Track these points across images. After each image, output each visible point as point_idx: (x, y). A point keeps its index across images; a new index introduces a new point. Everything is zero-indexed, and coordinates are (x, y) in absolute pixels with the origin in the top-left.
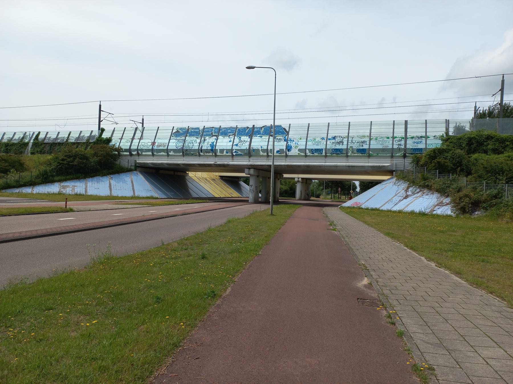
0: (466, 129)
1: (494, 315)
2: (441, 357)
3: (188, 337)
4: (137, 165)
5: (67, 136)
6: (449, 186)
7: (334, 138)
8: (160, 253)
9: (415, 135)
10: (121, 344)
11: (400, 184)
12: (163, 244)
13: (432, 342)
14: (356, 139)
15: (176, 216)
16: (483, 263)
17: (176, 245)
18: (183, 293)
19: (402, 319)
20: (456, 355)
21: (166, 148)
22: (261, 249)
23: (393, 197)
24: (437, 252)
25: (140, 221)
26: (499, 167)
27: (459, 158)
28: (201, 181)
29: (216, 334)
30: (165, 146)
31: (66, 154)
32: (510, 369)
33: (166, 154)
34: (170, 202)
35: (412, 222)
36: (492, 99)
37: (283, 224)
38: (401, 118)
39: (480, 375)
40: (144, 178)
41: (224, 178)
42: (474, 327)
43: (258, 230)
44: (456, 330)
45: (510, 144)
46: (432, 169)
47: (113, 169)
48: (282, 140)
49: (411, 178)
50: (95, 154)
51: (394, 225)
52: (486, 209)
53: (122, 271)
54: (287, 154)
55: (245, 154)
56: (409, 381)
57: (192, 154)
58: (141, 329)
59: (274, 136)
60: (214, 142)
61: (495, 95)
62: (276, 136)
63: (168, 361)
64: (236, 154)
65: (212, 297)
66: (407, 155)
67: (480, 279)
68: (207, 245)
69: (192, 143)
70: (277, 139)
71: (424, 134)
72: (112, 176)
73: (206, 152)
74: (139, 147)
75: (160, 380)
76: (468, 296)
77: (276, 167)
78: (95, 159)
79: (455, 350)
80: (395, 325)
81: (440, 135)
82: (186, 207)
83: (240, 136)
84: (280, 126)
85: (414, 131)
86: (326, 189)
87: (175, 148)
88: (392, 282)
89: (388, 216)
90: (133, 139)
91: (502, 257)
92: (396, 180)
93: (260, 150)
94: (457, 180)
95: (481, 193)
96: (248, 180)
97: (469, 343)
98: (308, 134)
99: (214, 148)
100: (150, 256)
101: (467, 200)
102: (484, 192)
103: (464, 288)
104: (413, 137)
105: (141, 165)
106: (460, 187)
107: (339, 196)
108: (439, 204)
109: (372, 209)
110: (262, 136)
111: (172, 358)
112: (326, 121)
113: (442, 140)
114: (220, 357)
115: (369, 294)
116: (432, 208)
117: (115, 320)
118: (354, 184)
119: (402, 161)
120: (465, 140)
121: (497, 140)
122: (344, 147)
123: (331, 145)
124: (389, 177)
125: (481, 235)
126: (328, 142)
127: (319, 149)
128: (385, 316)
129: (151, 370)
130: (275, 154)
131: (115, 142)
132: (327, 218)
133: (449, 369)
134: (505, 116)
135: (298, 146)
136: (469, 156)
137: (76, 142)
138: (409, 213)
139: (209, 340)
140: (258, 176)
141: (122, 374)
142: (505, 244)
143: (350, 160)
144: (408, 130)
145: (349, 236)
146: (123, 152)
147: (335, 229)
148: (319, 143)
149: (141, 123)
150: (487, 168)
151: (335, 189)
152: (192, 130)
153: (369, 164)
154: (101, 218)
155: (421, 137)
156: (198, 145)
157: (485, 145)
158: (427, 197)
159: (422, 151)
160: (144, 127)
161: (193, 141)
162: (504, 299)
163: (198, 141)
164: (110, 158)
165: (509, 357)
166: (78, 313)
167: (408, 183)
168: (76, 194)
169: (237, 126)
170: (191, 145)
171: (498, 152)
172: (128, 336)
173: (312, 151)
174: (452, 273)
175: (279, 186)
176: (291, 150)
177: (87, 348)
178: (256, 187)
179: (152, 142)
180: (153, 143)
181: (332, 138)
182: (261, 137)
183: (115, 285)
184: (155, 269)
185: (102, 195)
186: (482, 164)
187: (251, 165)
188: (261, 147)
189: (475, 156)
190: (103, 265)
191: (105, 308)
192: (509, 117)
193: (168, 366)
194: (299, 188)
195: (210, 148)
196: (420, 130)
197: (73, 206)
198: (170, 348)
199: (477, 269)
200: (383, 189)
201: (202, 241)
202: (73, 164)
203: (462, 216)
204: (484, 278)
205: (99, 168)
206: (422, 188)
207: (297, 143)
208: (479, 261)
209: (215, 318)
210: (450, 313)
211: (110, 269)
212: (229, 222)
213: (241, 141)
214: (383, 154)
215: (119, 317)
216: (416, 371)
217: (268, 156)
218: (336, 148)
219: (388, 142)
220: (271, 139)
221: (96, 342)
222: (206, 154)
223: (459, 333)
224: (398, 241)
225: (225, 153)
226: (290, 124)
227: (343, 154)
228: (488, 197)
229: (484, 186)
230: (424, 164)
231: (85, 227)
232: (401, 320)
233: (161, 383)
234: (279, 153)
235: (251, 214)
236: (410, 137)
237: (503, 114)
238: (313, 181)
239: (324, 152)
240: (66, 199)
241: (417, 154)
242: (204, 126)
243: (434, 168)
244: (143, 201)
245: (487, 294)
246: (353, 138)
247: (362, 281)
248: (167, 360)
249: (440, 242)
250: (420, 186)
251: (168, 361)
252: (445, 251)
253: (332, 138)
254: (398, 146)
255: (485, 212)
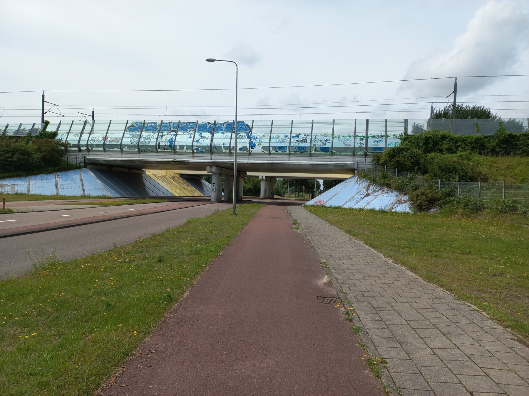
0: (423, 129)
1: (443, 307)
2: (393, 350)
3: (141, 345)
4: (87, 161)
5: (4, 128)
6: (407, 184)
7: (298, 136)
8: (112, 257)
9: (375, 134)
10: (64, 356)
11: (361, 183)
12: (116, 247)
13: (386, 336)
14: (319, 138)
15: (131, 217)
16: (436, 258)
17: (130, 247)
18: (136, 299)
19: (359, 315)
20: (407, 347)
21: (119, 143)
22: (222, 249)
23: (355, 196)
24: (394, 248)
25: (90, 222)
26: (452, 166)
27: (416, 156)
28: (159, 179)
29: (171, 341)
30: (118, 141)
31: (3, 149)
32: (454, 358)
33: (120, 150)
34: (125, 201)
35: (372, 220)
36: (446, 100)
37: (246, 224)
38: (362, 118)
39: (427, 365)
40: (96, 176)
41: (184, 176)
42: (424, 320)
43: (219, 230)
44: (408, 323)
45: (462, 144)
46: (391, 168)
47: (59, 166)
48: (245, 136)
49: (372, 176)
50: (39, 150)
51: (355, 223)
52: (440, 206)
53: (69, 277)
54: (251, 151)
55: (207, 151)
56: (363, 375)
57: (149, 151)
58: (88, 339)
59: (236, 133)
60: (173, 138)
61: (449, 97)
62: (239, 132)
63: (118, 371)
64: (197, 151)
65: (168, 301)
66: (368, 153)
67: (432, 274)
68: (165, 247)
69: (149, 138)
70: (240, 136)
71: (384, 133)
72: (58, 174)
73: (165, 149)
74: (89, 142)
75: (108, 392)
76: (421, 290)
77: (239, 164)
78: (39, 155)
79: (406, 343)
80: (352, 321)
81: (399, 134)
82: (143, 207)
83: (201, 132)
84: (243, 123)
85: (375, 130)
86: (290, 187)
87: (129, 143)
88: (351, 279)
89: (350, 214)
90: (82, 133)
91: (453, 252)
92: (358, 178)
93: (222, 147)
94: (415, 178)
95: (436, 190)
96: (210, 178)
97: (419, 335)
98: (271, 131)
99: (173, 145)
100: (101, 260)
101: (424, 198)
102: (439, 189)
103: (418, 282)
104: (373, 136)
105: (91, 162)
106: (418, 185)
107: (303, 194)
108: (398, 202)
109: (335, 208)
110: (224, 132)
111: (123, 368)
112: (290, 118)
113: (401, 140)
114: (174, 364)
115: (329, 292)
116: (391, 205)
117: (59, 331)
118: (318, 182)
119: (363, 160)
120: (422, 139)
121: (451, 140)
122: (308, 145)
123: (294, 143)
124: (351, 175)
125: (436, 232)
126: (292, 140)
127: (283, 147)
128: (343, 313)
129: (98, 382)
130: (238, 151)
131: (61, 136)
132: (290, 217)
133: (400, 361)
134: (458, 117)
135: (261, 143)
136: (426, 155)
137: (15, 135)
138: (369, 211)
139: (163, 347)
140: (220, 174)
141: (65, 388)
142: (456, 239)
143: (314, 158)
144: (369, 129)
145: (312, 234)
146: (70, 147)
147: (298, 228)
148: (282, 141)
149: (91, 116)
150: (442, 167)
151: (299, 187)
152: (149, 125)
153: (332, 163)
154: (45, 220)
155: (382, 136)
156: (156, 140)
157: (440, 145)
158: (387, 195)
159: (382, 150)
160: (95, 121)
161: (150, 137)
162: (452, 292)
163: (156, 136)
164: (56, 154)
165: (454, 347)
166: (15, 325)
167: (369, 181)
168: (17, 194)
169: (197, 121)
170: (148, 140)
171: (451, 151)
172: (73, 347)
173: (276, 149)
174: (407, 269)
175: (242, 184)
176: (255, 147)
177: (25, 363)
178: (218, 185)
179: (103, 137)
180: (105, 138)
181: (296, 136)
182: (223, 133)
183: (60, 293)
184: (105, 274)
185: (47, 195)
186: (438, 163)
187: (213, 163)
188: (224, 144)
189: (431, 155)
190: (47, 271)
191: (48, 318)
192: (461, 118)
193: (117, 376)
194: (263, 187)
195: (169, 144)
196: (380, 129)
197: (12, 207)
198: (119, 357)
199: (431, 264)
200: (345, 187)
201: (159, 243)
202: (12, 160)
203: (419, 214)
204: (436, 272)
205: (43, 165)
206: (382, 186)
207: (260, 141)
208: (432, 257)
209: (171, 323)
210: (404, 307)
211: (55, 275)
212: (189, 222)
213: (202, 138)
214: (345, 152)
215: (64, 326)
216: (369, 365)
217: (231, 153)
218: (300, 146)
219: (350, 140)
220: (234, 135)
221: (35, 356)
222: (164, 151)
223: (411, 326)
224: (358, 239)
225: (185, 150)
226: (253, 121)
227: (306, 152)
228: (443, 195)
229: (439, 184)
230: (384, 163)
231: (26, 230)
232: (358, 317)
233: (109, 395)
234: (242, 150)
235: (213, 213)
236: (371, 136)
237: (457, 115)
238: (277, 179)
239: (288, 150)
240: (4, 199)
241: (378, 152)
242: (162, 121)
243: (393, 167)
244: (94, 201)
245: (438, 287)
246: (316, 136)
247: (322, 279)
248: (116, 370)
249: (398, 239)
250: (380, 184)
251: (118, 371)
252: (402, 248)
253: (296, 136)
254: (359, 145)
255: (440, 209)
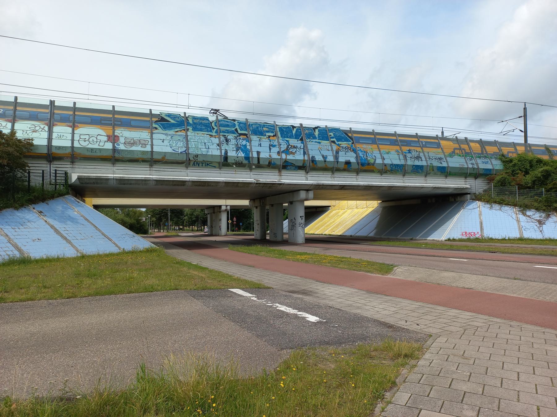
70: (343, 147)
127: (399, 165)
